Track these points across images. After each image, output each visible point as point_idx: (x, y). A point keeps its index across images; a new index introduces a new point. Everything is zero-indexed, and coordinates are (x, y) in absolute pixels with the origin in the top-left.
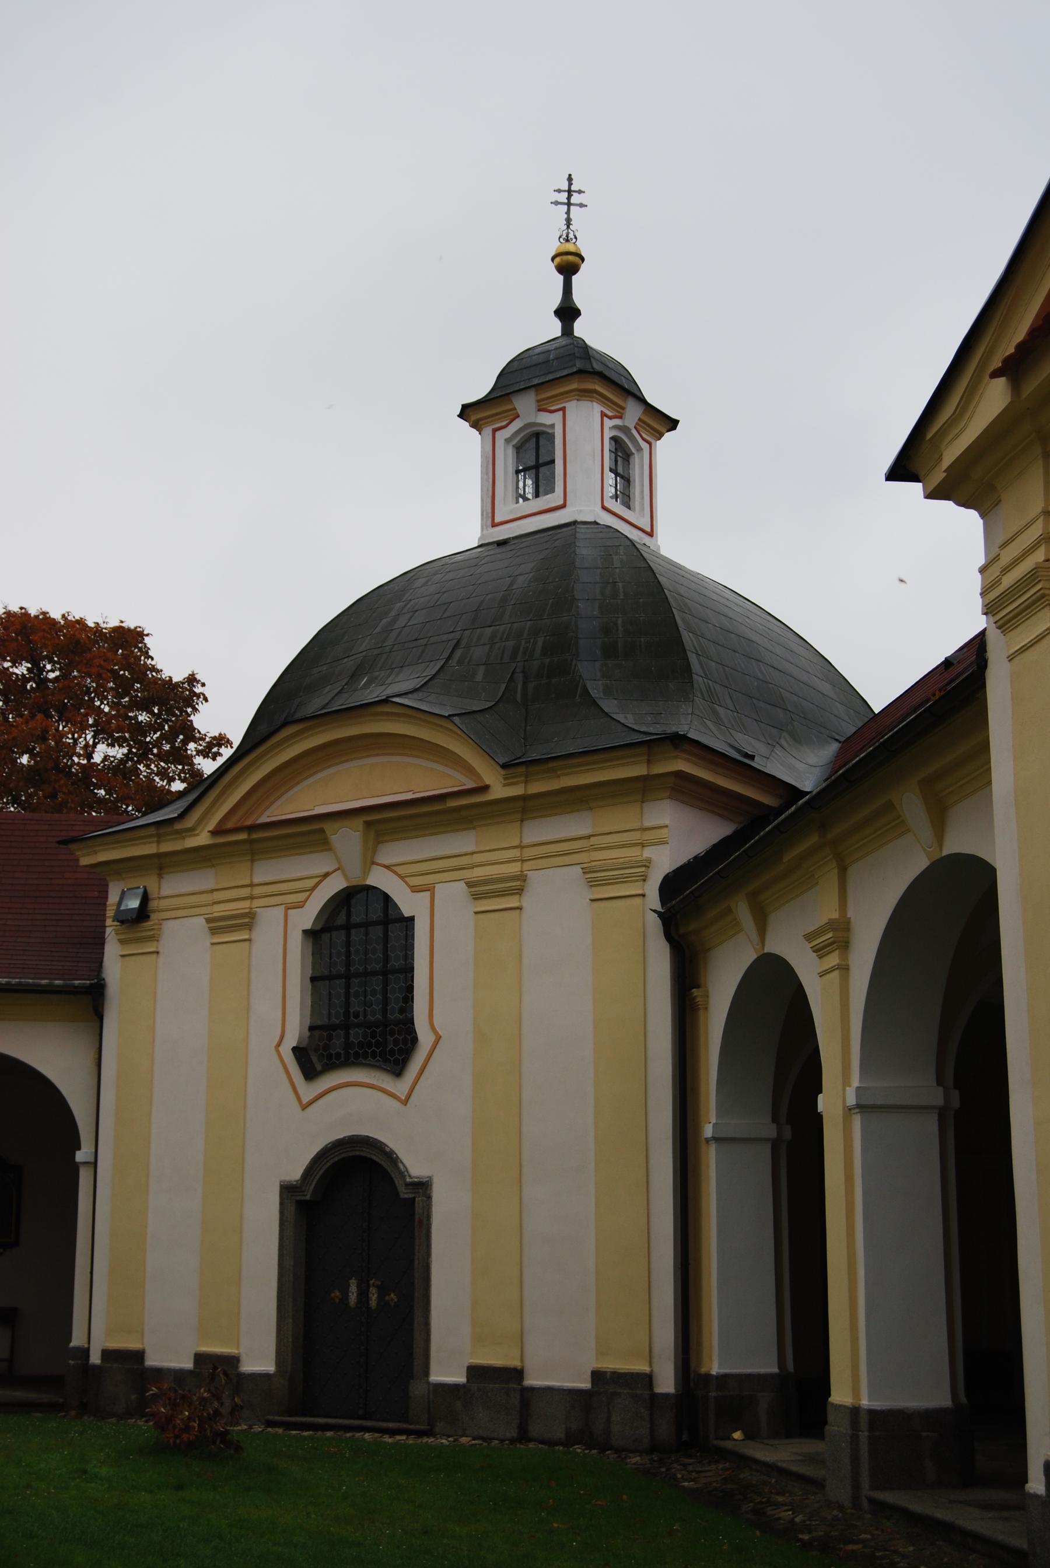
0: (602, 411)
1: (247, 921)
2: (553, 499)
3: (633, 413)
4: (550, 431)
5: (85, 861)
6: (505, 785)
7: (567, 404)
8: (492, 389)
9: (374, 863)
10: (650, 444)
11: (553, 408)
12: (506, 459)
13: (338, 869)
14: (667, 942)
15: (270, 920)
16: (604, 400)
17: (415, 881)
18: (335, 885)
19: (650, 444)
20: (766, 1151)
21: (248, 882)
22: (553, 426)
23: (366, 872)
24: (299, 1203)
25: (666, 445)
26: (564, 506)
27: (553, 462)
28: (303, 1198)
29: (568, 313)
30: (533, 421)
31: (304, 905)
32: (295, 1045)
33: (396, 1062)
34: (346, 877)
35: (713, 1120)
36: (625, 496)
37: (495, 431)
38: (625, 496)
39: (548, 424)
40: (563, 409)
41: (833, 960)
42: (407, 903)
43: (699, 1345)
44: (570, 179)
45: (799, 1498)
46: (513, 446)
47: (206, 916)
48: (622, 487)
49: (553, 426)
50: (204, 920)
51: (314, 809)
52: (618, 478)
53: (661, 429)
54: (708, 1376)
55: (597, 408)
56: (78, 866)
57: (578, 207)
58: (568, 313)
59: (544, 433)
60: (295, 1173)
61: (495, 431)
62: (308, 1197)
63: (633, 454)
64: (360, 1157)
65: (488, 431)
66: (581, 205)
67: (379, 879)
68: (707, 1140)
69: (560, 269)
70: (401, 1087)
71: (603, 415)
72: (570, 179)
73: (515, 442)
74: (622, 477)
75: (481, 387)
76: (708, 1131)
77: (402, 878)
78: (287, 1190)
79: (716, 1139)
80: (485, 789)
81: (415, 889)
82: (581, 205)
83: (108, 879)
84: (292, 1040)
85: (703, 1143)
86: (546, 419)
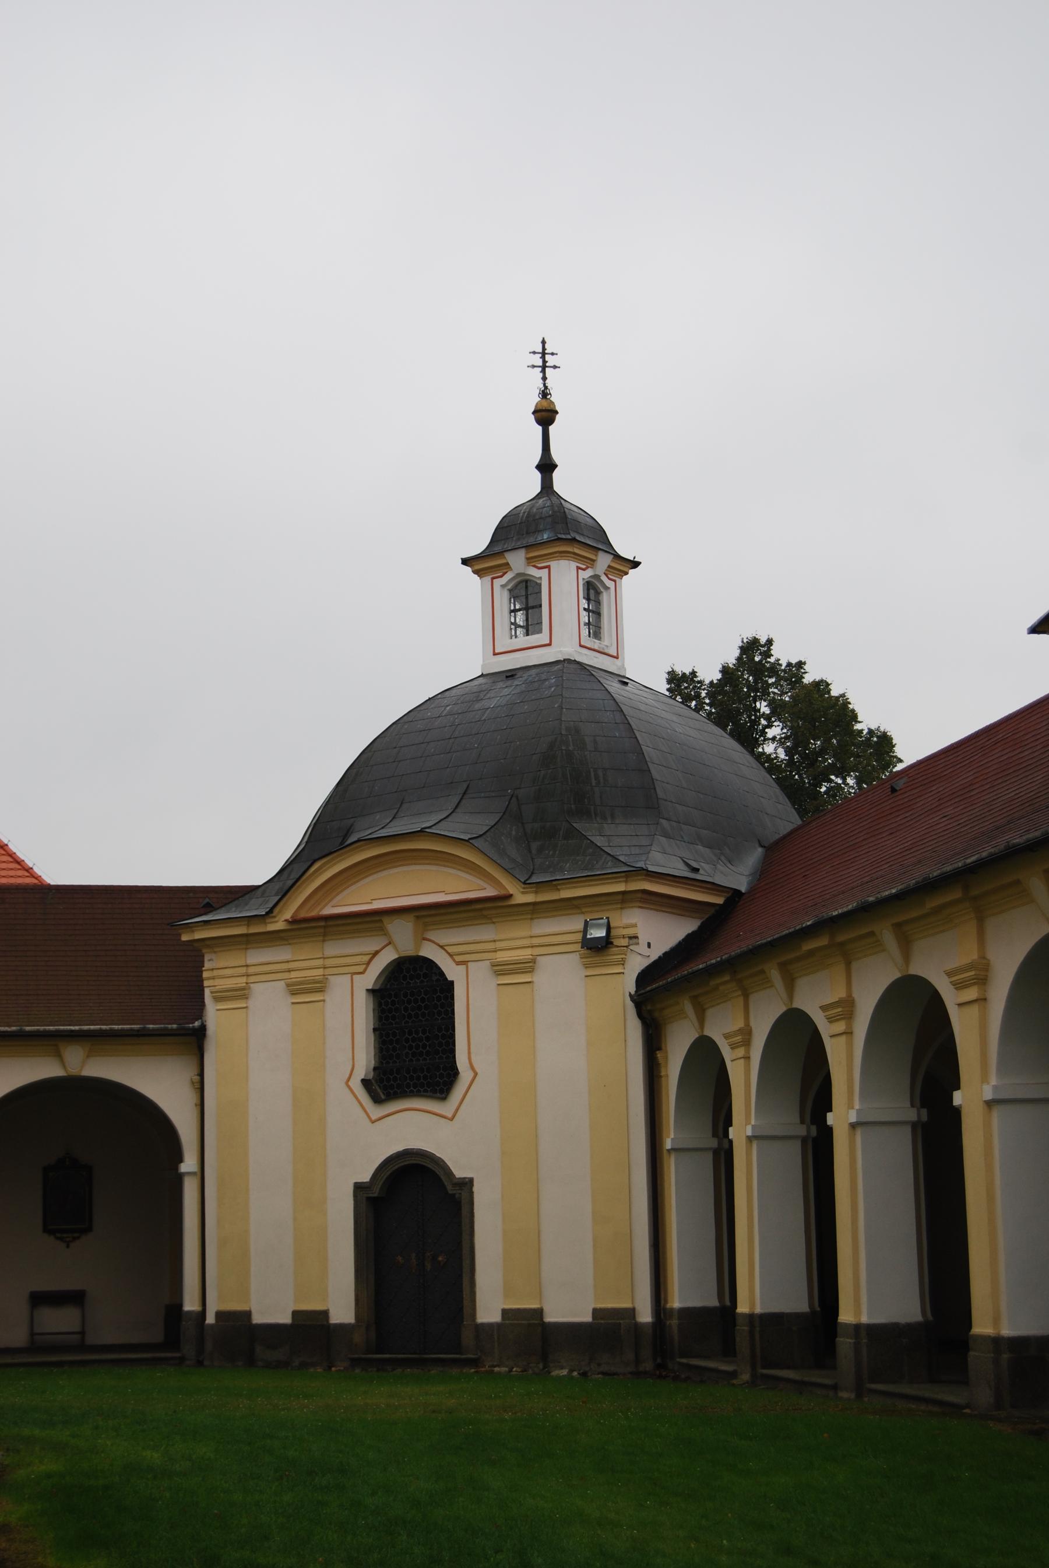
0: (577, 567)
1: (319, 987)
2: (542, 638)
3: (604, 561)
4: (538, 582)
5: (185, 938)
6: (523, 893)
7: (552, 562)
8: (490, 543)
9: (425, 939)
10: (615, 581)
11: (539, 565)
12: (502, 599)
13: (390, 943)
14: (638, 1019)
15: (340, 985)
16: (577, 557)
17: (458, 958)
18: (388, 956)
19: (615, 581)
20: (710, 1156)
21: (321, 956)
22: (540, 578)
23: (418, 947)
24: (368, 1199)
25: (630, 580)
26: (550, 644)
27: (540, 606)
28: (371, 1195)
29: (547, 467)
30: (523, 572)
31: (365, 970)
32: (363, 1077)
33: (442, 1091)
34: (396, 949)
35: (672, 1136)
36: (595, 629)
37: (493, 579)
38: (595, 629)
39: (537, 576)
40: (548, 567)
41: (972, 994)
42: (451, 971)
43: (665, 1277)
44: (544, 342)
45: (554, 680)
46: (508, 590)
47: (286, 981)
48: (594, 619)
49: (540, 578)
50: (284, 984)
51: (372, 900)
52: (591, 614)
53: (625, 569)
54: (672, 1309)
55: (573, 565)
56: (180, 940)
57: (552, 369)
58: (547, 467)
59: (531, 581)
60: (365, 1177)
61: (493, 579)
62: (376, 1195)
63: (602, 592)
64: (413, 1165)
65: (488, 579)
66: (555, 367)
67: (428, 951)
68: (669, 1151)
69: (539, 421)
70: (446, 1108)
71: (578, 568)
72: (544, 342)
73: (509, 587)
74: (593, 612)
75: (479, 544)
76: (668, 1144)
77: (451, 955)
78: (358, 1187)
79: (673, 1150)
80: (510, 896)
81: (458, 963)
82: (555, 367)
83: (204, 951)
84: (361, 1073)
85: (665, 1152)
86: (533, 572)
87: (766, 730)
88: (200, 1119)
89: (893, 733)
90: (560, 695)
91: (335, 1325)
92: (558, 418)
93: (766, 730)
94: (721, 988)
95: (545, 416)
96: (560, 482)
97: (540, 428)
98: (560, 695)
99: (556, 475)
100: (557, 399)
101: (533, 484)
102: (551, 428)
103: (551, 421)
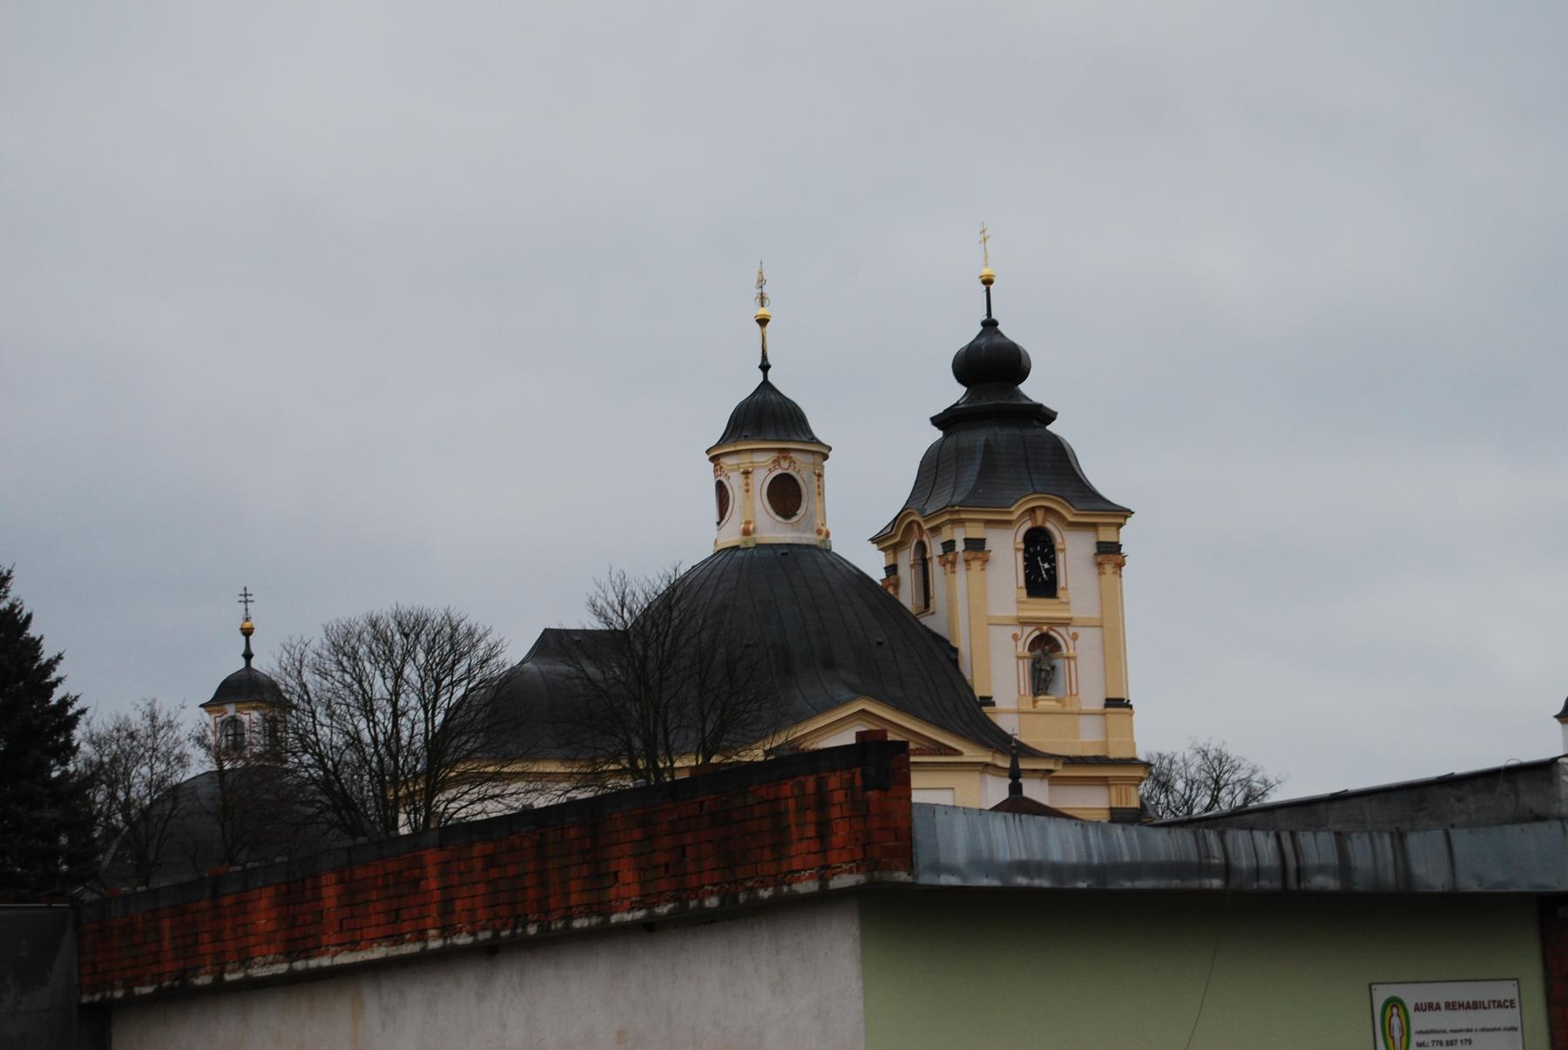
29: (248, 656)
32: (884, 566)
58: (248, 656)
72: (245, 589)
87: (79, 716)
88: (922, 579)
89: (995, 282)
90: (841, 807)
91: (1019, 390)
92: (255, 631)
93: (79, 716)
94: (794, 455)
95: (247, 633)
96: (255, 664)
97: (244, 638)
98: (841, 807)
99: (770, 372)
100: (253, 622)
101: (241, 664)
102: (251, 637)
103: (251, 633)
